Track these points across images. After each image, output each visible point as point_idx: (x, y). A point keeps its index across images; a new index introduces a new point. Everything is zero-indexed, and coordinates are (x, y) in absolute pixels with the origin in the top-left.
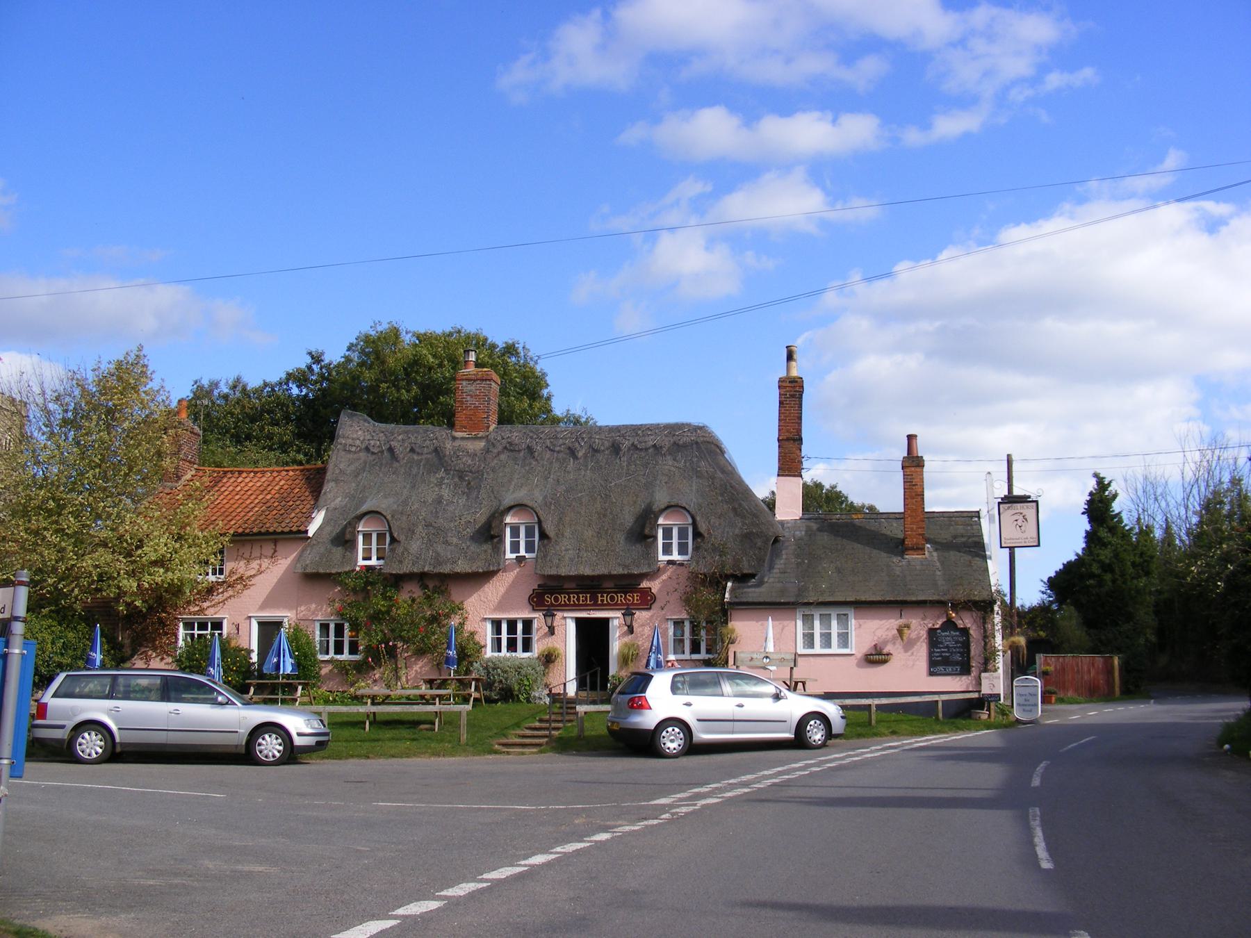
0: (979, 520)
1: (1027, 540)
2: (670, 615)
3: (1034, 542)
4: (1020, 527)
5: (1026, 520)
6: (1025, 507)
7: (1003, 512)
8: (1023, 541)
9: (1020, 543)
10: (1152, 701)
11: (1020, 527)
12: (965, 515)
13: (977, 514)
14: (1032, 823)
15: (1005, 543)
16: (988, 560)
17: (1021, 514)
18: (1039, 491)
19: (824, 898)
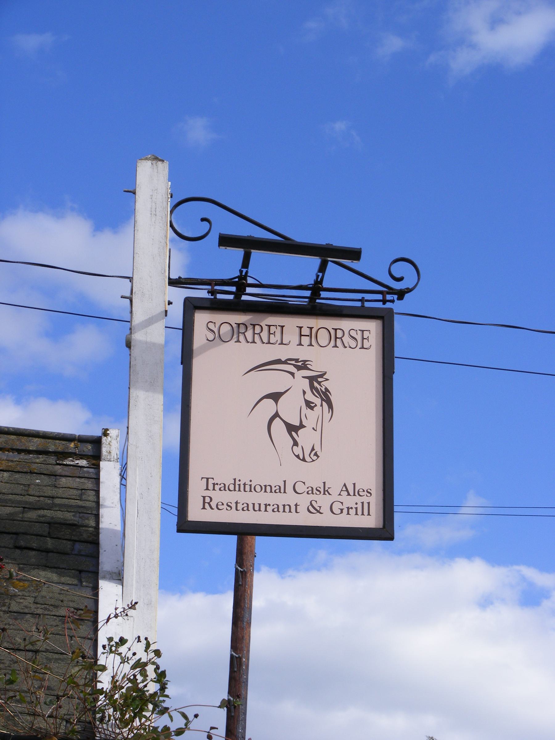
0: (97, 467)
1: (323, 501)
2: (50, 673)
3: (364, 510)
4: (292, 429)
5: (326, 397)
6: (323, 337)
7: (204, 349)
8: (304, 501)
9: (286, 508)
10: (23, 547)
11: (292, 429)
12: (34, 444)
13: (88, 448)
14: (135, 323)
15: (206, 503)
16: (103, 584)
17: (303, 366)
18: (400, 269)
19: (329, 420)
